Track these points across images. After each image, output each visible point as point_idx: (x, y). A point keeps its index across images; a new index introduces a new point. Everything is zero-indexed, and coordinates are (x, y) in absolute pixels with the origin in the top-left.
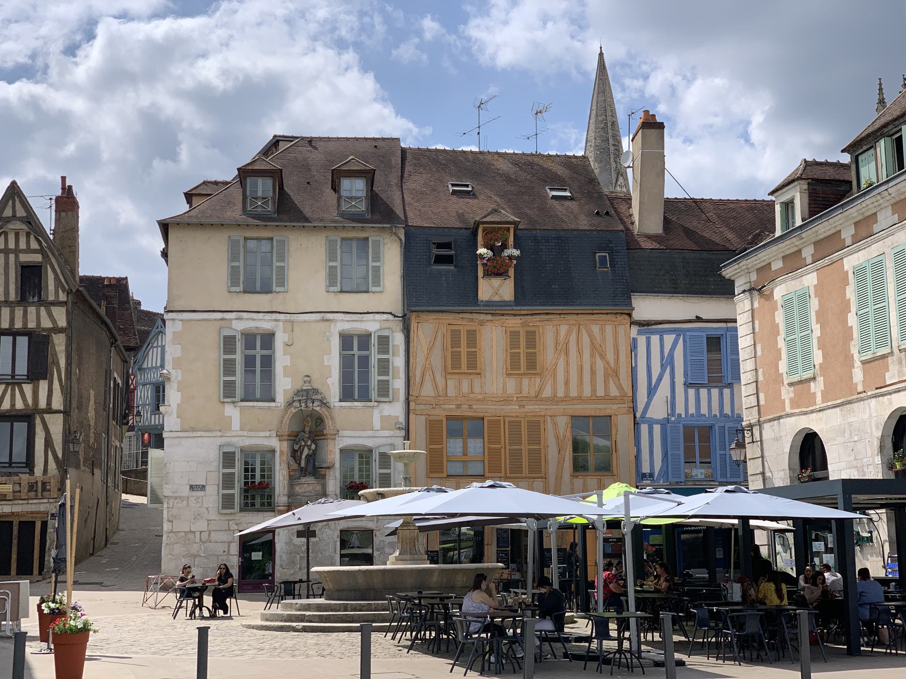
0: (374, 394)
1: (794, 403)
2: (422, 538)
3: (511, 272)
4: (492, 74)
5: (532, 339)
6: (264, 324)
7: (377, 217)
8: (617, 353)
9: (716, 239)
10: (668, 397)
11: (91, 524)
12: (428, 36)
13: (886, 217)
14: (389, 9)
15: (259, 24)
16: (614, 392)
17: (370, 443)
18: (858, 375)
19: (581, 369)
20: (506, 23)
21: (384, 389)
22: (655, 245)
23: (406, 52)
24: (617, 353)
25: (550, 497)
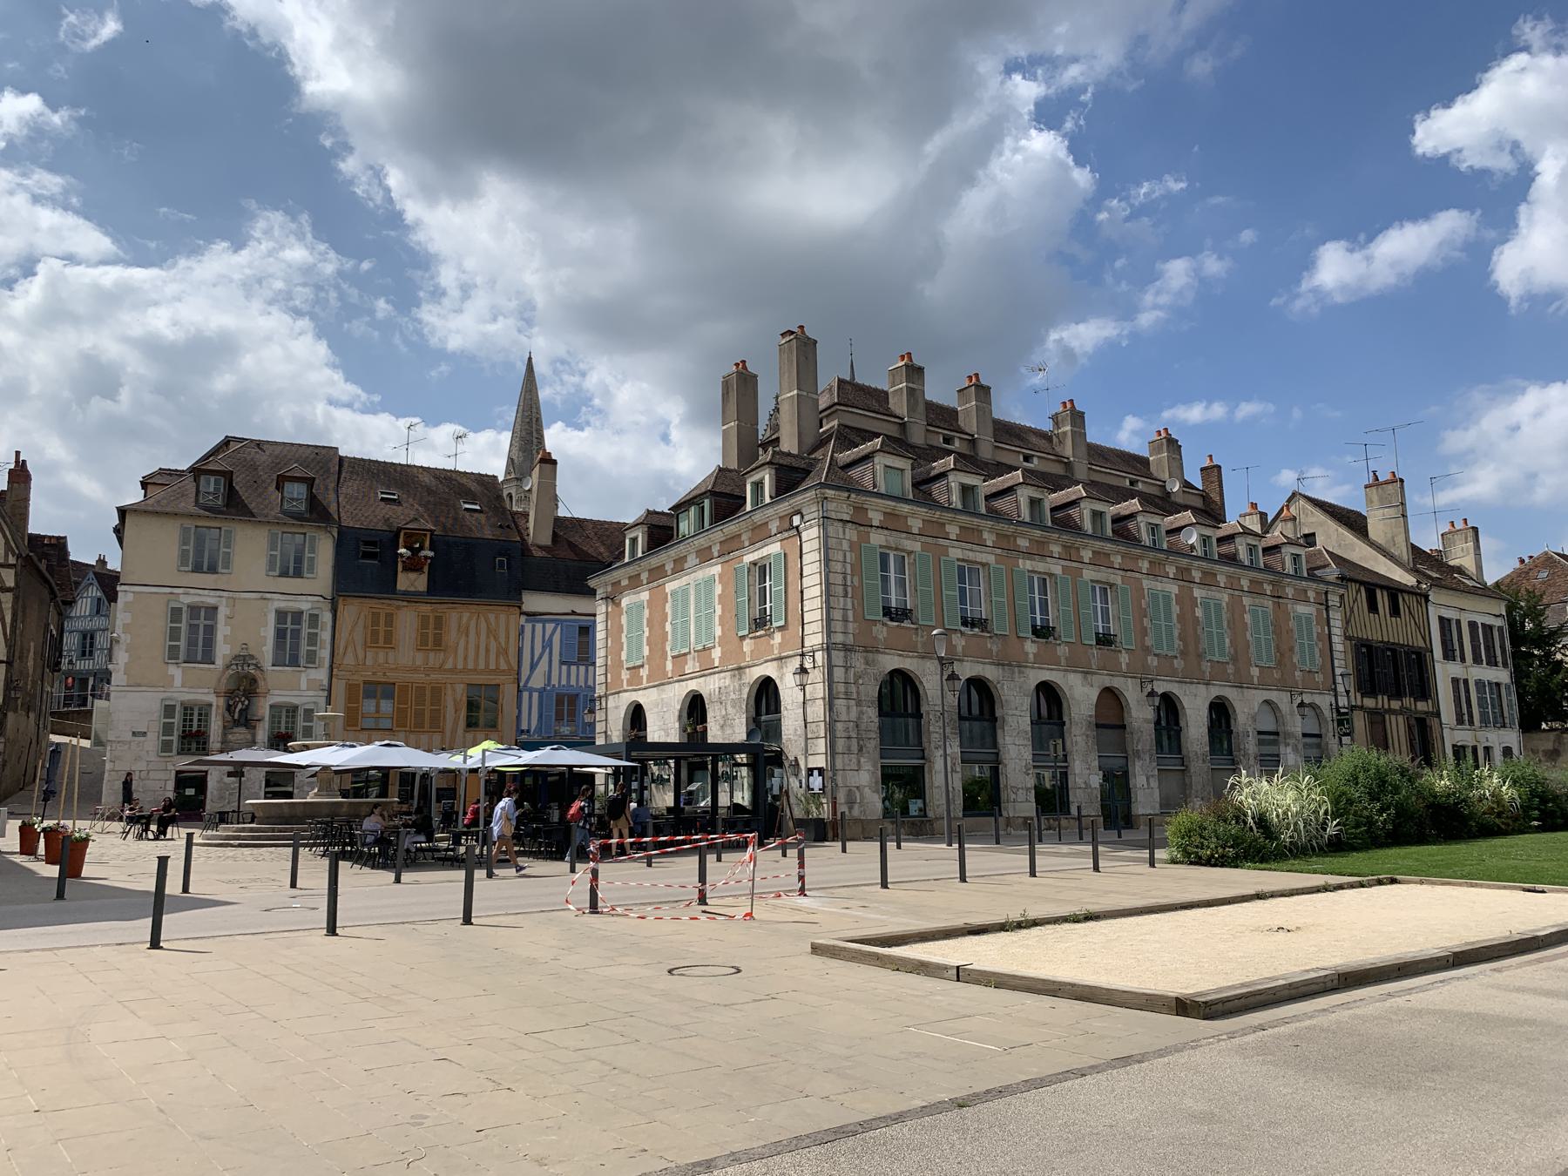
0: (302, 661)
1: (630, 683)
2: (337, 779)
3: (426, 569)
4: (442, 355)
5: (439, 622)
6: (209, 599)
7: (314, 516)
8: (508, 637)
9: (591, 551)
10: (546, 673)
11: (23, 761)
12: (380, 315)
13: (692, 560)
14: (345, 286)
15: (214, 285)
16: (503, 666)
17: (295, 701)
18: (669, 665)
19: (478, 647)
20: (459, 311)
21: (312, 658)
22: (544, 554)
23: (358, 327)
24: (508, 637)
25: (419, 752)
